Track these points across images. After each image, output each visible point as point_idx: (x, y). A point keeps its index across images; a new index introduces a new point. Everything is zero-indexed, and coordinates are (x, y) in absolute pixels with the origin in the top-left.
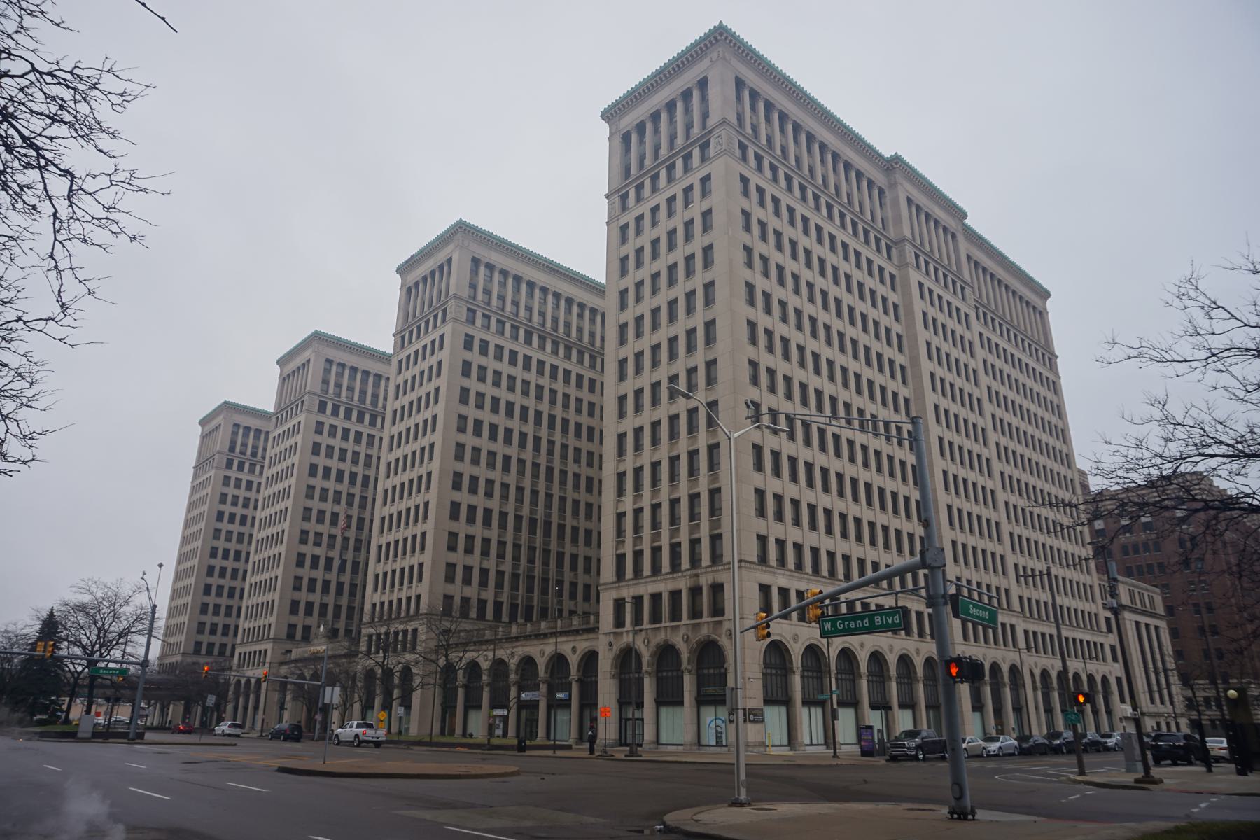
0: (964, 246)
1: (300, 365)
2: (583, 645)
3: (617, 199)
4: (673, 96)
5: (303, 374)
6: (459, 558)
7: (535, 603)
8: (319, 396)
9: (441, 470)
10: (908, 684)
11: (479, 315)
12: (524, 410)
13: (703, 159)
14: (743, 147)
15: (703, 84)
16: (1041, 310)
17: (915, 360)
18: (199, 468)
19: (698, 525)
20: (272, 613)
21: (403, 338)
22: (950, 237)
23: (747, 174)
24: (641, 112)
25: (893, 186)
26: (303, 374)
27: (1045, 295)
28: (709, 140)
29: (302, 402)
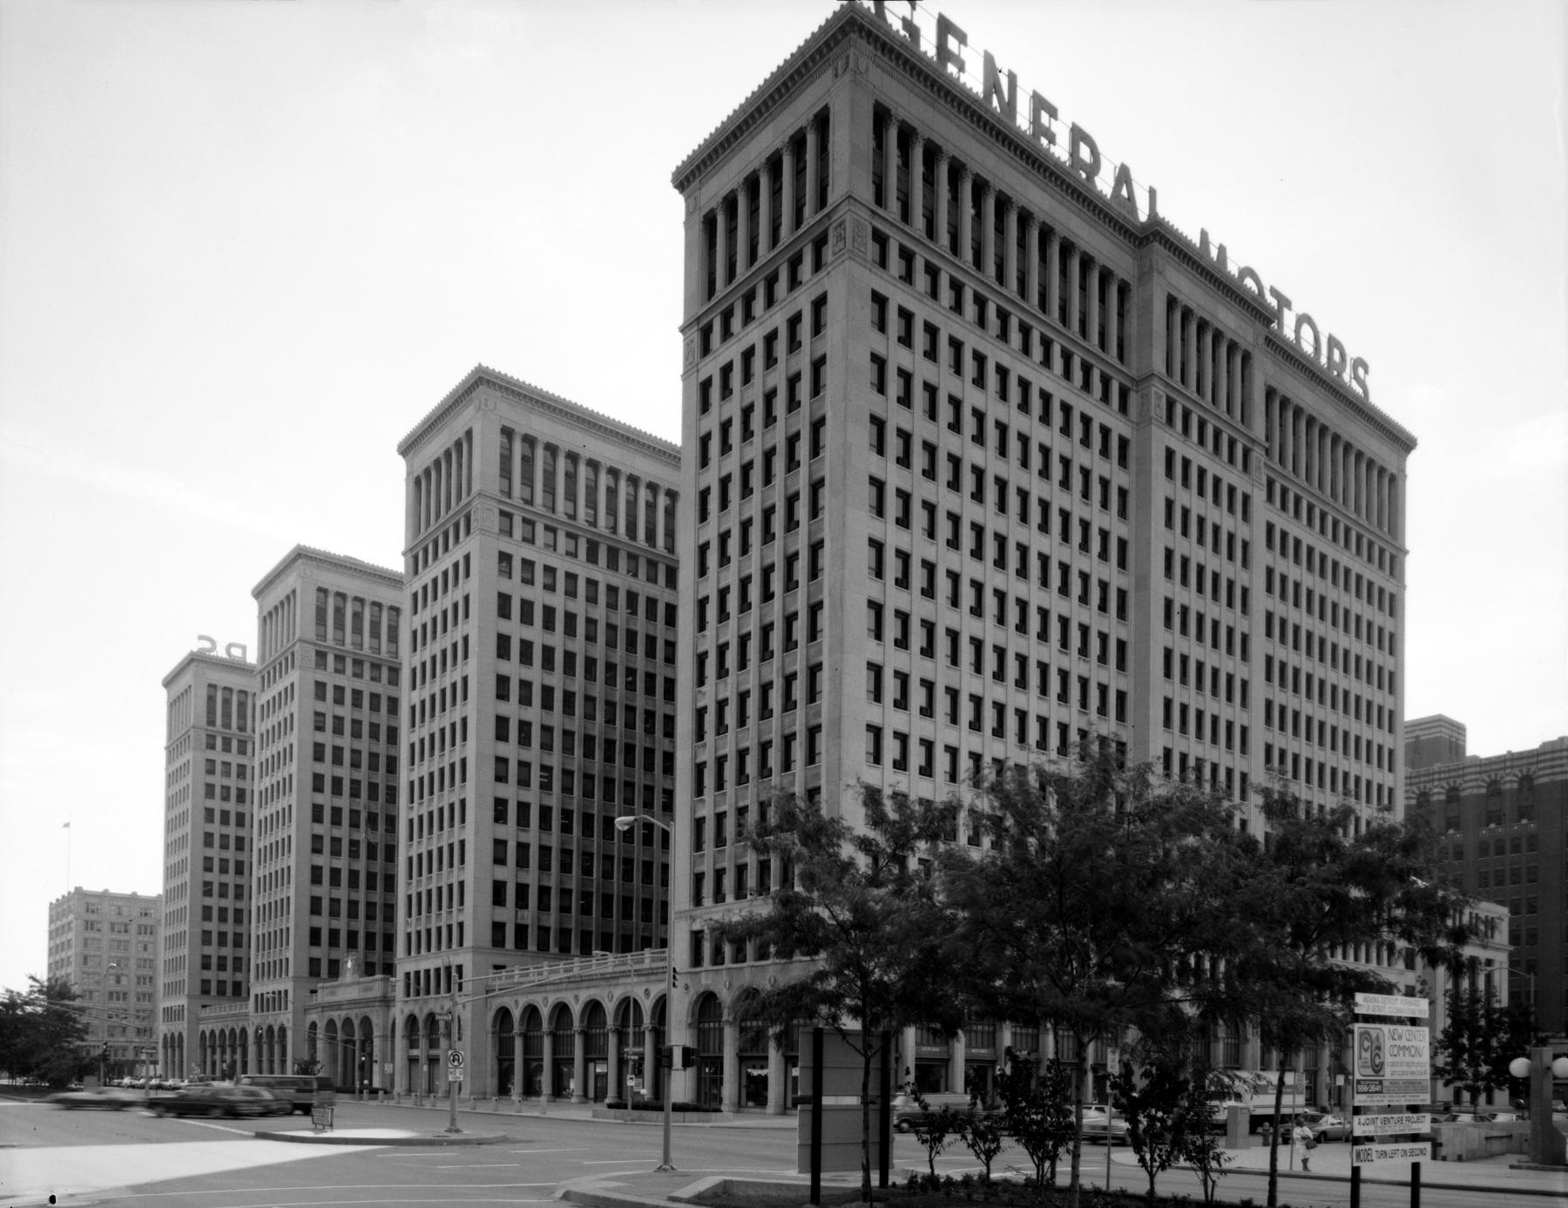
0: (1265, 371)
1: (282, 597)
2: (656, 990)
3: (696, 335)
4: (779, 146)
5: (449, 475)
6: (211, 975)
7: (615, 930)
8: (315, 644)
9: (479, 755)
10: (1032, 1035)
11: (517, 521)
12: (547, 692)
13: (818, 265)
14: (880, 239)
15: (822, 121)
16: (1394, 471)
17: (1143, 583)
18: (173, 750)
19: (724, 851)
20: (288, 944)
21: (416, 558)
22: (1386, 481)
23: (884, 289)
24: (728, 177)
25: (1144, 276)
26: (449, 475)
27: (1404, 443)
28: (826, 231)
29: (293, 655)
